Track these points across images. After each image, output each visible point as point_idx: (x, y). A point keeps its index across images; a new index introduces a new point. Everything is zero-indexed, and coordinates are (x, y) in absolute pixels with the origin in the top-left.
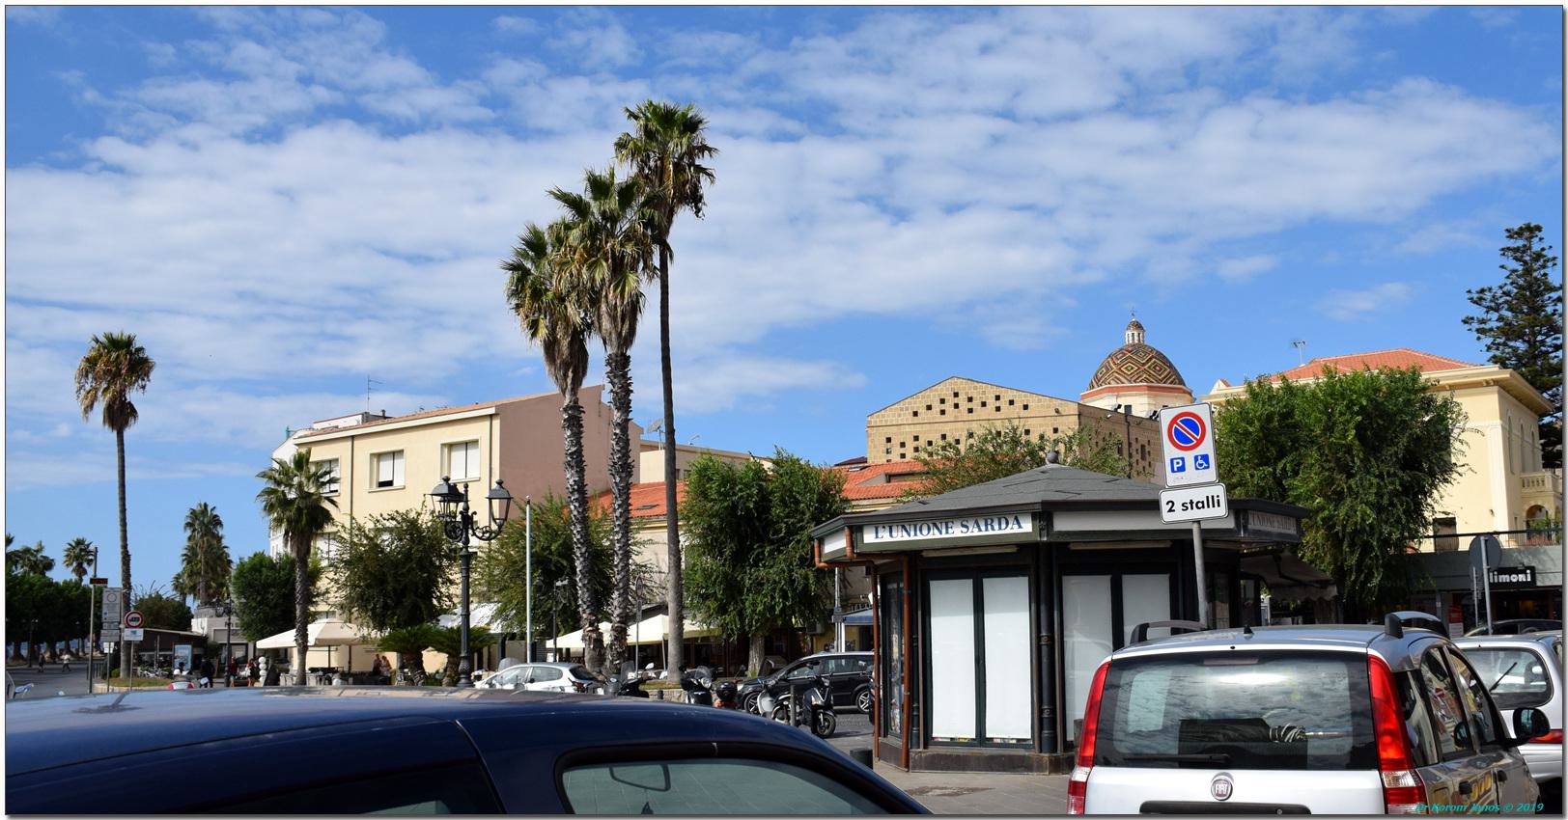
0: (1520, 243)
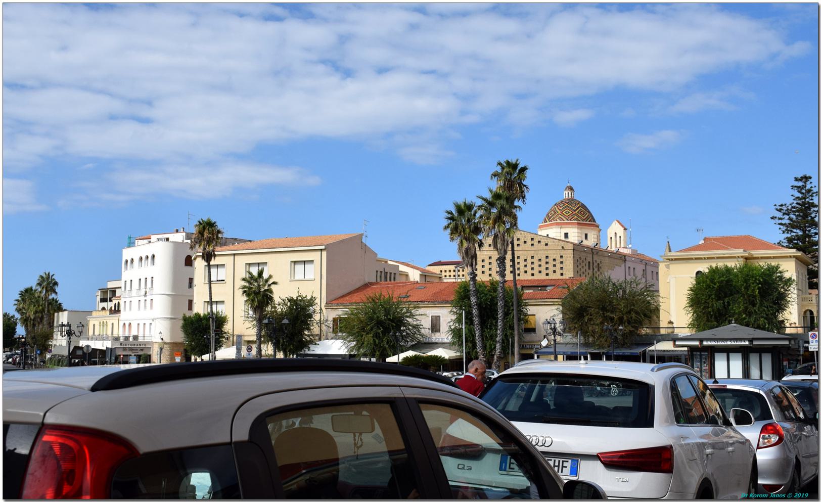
0: (800, 184)
